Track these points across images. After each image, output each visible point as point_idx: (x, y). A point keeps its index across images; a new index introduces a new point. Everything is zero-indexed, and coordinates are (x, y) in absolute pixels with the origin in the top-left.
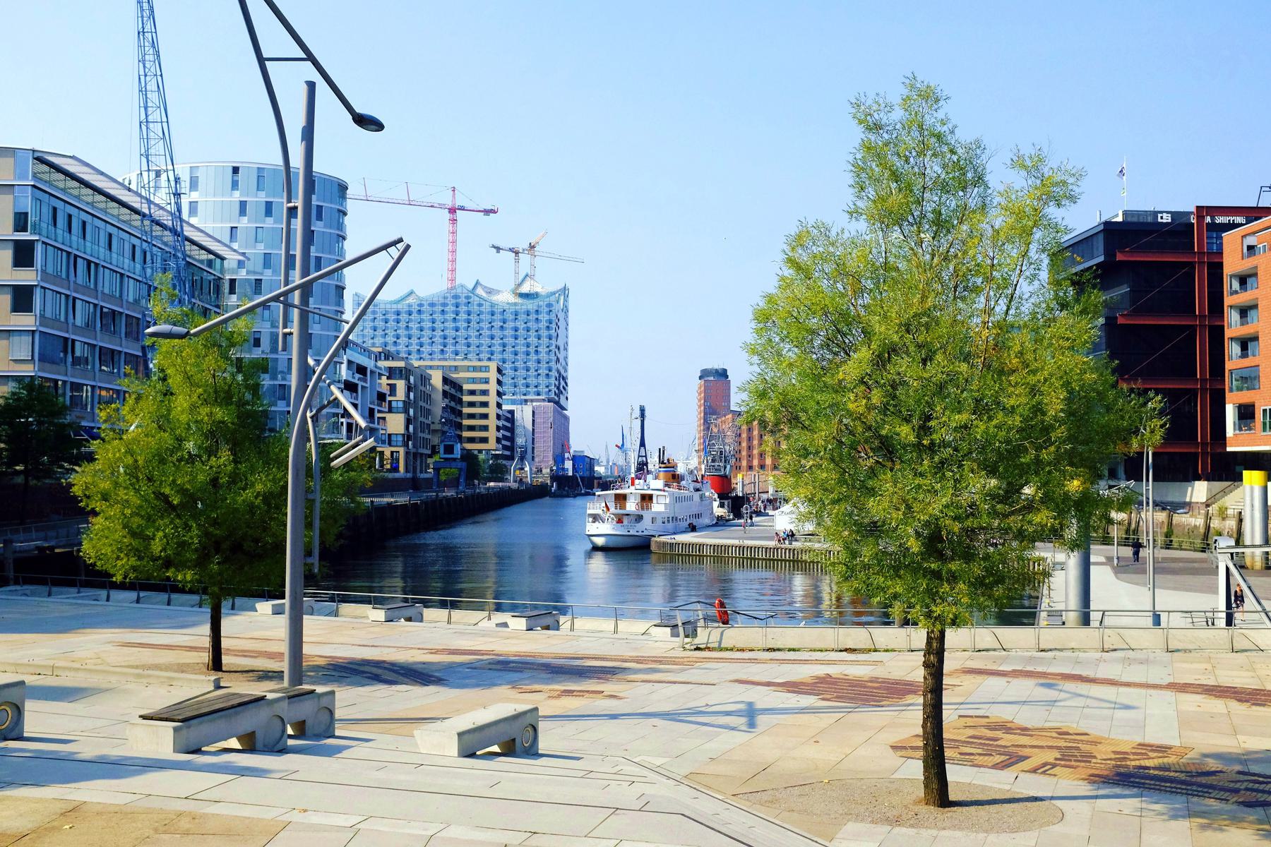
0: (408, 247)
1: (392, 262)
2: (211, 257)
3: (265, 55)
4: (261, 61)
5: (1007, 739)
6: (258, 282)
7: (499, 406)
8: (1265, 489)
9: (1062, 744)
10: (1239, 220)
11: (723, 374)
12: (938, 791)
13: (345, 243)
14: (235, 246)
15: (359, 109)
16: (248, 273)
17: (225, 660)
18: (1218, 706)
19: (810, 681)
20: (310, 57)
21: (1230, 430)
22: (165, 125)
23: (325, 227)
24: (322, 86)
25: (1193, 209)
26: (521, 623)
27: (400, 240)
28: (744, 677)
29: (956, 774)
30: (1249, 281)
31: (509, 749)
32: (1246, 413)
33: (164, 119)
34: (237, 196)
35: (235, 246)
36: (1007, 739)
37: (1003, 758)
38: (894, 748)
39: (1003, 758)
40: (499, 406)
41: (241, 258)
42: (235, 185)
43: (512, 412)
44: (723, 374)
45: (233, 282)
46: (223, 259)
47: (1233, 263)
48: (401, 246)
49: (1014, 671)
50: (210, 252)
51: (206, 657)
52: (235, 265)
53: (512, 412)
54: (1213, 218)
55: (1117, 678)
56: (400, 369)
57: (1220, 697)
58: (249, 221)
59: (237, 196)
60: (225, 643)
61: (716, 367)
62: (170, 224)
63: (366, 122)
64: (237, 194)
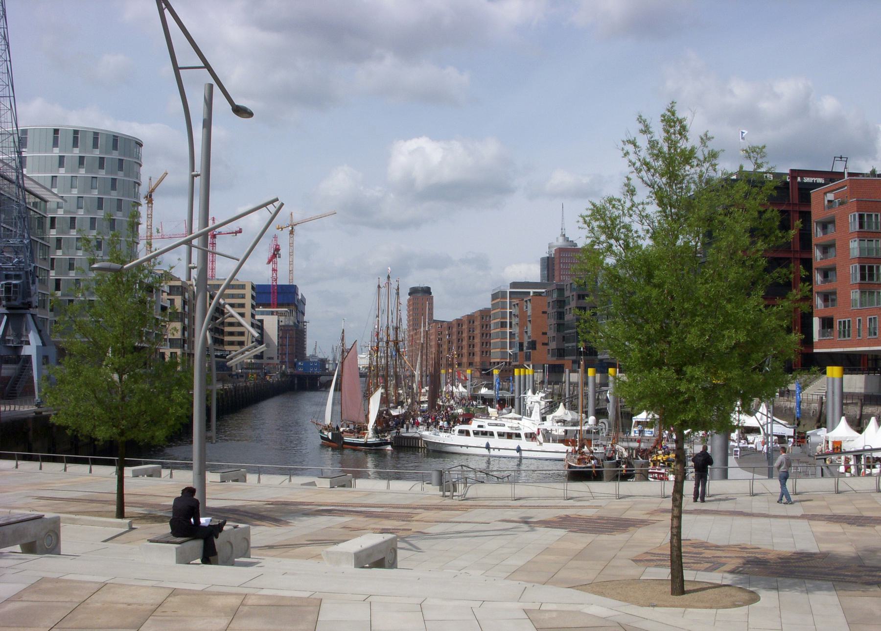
0: (282, 204)
1: (270, 216)
2: (38, 200)
3: (179, 66)
4: (177, 69)
5: (708, 553)
6: (73, 219)
7: (253, 316)
8: (842, 380)
9: (745, 555)
10: (820, 180)
11: (427, 291)
12: (678, 586)
13: (141, 187)
14: (55, 191)
15: (238, 102)
16: (65, 212)
17: (127, 509)
18: (836, 528)
19: (555, 519)
20: (207, 66)
21: (816, 337)
22: (12, 98)
23: (125, 176)
24: (216, 88)
25: (788, 171)
26: (325, 483)
27: (277, 200)
28: (508, 518)
29: (688, 575)
30: (830, 226)
31: (379, 564)
32: (827, 323)
33: (12, 94)
34: (56, 152)
35: (55, 191)
36: (708, 553)
37: (709, 565)
38: (636, 561)
39: (709, 565)
40: (253, 316)
41: (60, 200)
42: (55, 144)
43: (261, 321)
44: (427, 291)
45: (53, 219)
46: (46, 201)
47: (817, 213)
48: (277, 204)
49: (696, 510)
50: (36, 196)
51: (114, 508)
52: (55, 206)
53: (261, 321)
54: (802, 179)
55: (767, 513)
56: (178, 287)
57: (837, 522)
58: (66, 172)
59: (56, 152)
60: (127, 499)
61: (422, 286)
62: (14, 178)
63: (241, 111)
64: (56, 150)
